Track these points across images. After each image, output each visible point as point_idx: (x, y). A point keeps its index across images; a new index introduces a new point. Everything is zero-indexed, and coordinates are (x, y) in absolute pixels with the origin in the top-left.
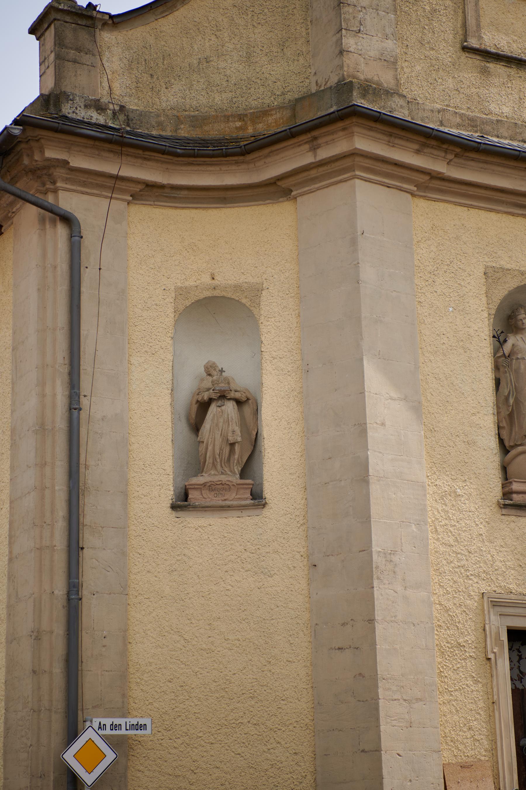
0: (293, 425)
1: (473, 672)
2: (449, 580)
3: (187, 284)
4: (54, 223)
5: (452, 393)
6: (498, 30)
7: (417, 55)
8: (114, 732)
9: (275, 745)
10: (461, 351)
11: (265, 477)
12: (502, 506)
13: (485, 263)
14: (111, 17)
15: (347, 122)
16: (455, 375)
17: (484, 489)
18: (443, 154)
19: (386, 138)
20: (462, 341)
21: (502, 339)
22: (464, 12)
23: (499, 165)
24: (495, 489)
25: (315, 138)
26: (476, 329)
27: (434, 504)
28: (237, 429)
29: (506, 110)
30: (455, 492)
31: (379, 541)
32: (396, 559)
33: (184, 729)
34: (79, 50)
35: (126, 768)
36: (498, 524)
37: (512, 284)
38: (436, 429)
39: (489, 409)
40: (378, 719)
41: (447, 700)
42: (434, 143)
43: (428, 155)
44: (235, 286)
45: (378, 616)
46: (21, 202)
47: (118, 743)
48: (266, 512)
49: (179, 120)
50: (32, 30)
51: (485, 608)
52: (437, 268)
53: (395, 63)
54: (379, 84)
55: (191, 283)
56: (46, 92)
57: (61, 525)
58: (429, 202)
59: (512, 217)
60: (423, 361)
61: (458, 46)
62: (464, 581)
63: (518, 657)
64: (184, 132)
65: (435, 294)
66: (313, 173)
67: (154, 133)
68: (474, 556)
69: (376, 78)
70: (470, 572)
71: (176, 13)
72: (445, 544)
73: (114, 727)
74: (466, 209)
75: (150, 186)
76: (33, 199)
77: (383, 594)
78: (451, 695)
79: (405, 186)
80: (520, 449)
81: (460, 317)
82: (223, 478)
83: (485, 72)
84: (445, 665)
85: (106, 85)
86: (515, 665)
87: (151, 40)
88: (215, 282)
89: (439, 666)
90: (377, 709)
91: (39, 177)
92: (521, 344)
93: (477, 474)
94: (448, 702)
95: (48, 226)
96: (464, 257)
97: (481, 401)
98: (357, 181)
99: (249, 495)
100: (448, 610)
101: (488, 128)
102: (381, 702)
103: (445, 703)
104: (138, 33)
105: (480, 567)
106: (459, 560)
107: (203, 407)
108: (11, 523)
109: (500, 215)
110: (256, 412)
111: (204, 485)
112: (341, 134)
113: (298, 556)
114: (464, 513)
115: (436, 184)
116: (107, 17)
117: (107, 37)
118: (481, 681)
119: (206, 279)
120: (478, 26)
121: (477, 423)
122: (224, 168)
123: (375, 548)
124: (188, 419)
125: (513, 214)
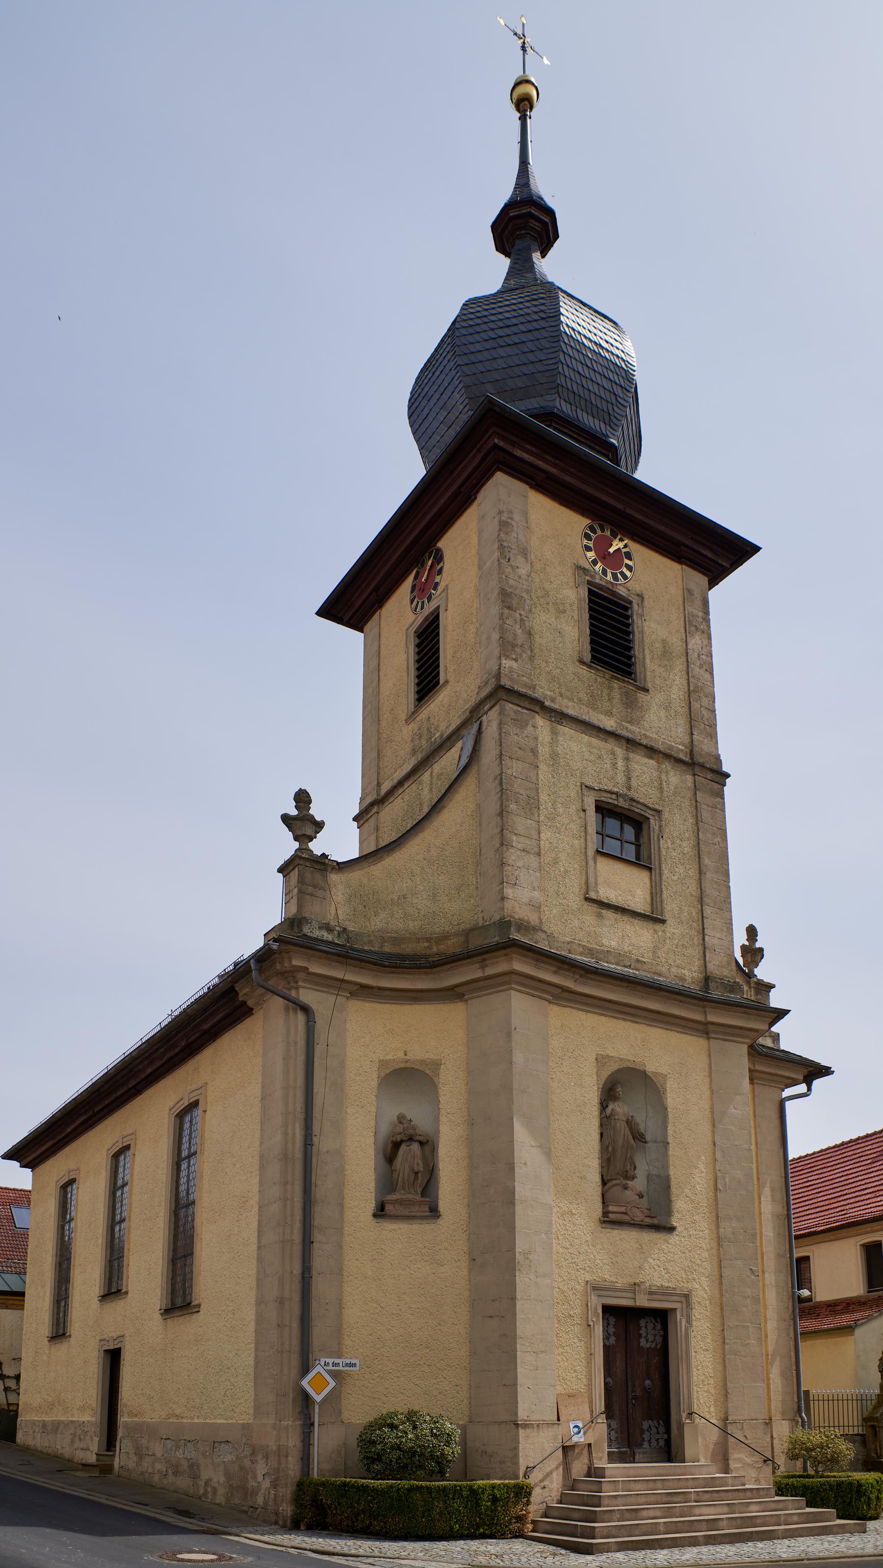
0: (461, 1161)
3: (387, 1057)
4: (295, 1011)
6: (610, 887)
7: (554, 902)
8: (334, 1368)
9: (442, 1379)
10: (579, 1113)
11: (440, 1197)
14: (338, 863)
15: (508, 950)
19: (534, 963)
21: (604, 1105)
22: (587, 873)
25: (484, 960)
28: (420, 1162)
29: (614, 944)
31: (521, 1245)
32: (530, 1257)
33: (380, 1367)
34: (315, 886)
35: (341, 1392)
37: (614, 1067)
40: (516, 1365)
42: (566, 967)
44: (421, 1061)
45: (518, 1296)
46: (270, 994)
47: (335, 1375)
48: (440, 1221)
49: (383, 940)
50: (280, 870)
53: (539, 907)
54: (528, 922)
55: (390, 1057)
56: (290, 915)
57: (298, 1226)
61: (582, 897)
64: (387, 948)
66: (481, 984)
67: (366, 948)
69: (526, 918)
71: (383, 862)
73: (334, 1364)
75: (363, 987)
76: (282, 994)
77: (522, 1281)
79: (545, 996)
80: (614, 1182)
82: (410, 1196)
83: (600, 916)
85: (333, 912)
87: (365, 881)
88: (407, 1057)
90: (516, 1358)
91: (286, 978)
92: (618, 1109)
95: (291, 1013)
98: (513, 992)
99: (427, 1209)
101: (601, 956)
102: (518, 1353)
104: (356, 875)
106: (573, 1258)
107: (396, 1145)
108: (260, 1221)
110: (434, 1150)
111: (397, 1200)
112: (503, 958)
113: (462, 1253)
115: (566, 995)
116: (335, 864)
117: (334, 878)
119: (401, 1055)
120: (596, 884)
122: (417, 976)
123: (518, 1250)
124: (384, 1154)
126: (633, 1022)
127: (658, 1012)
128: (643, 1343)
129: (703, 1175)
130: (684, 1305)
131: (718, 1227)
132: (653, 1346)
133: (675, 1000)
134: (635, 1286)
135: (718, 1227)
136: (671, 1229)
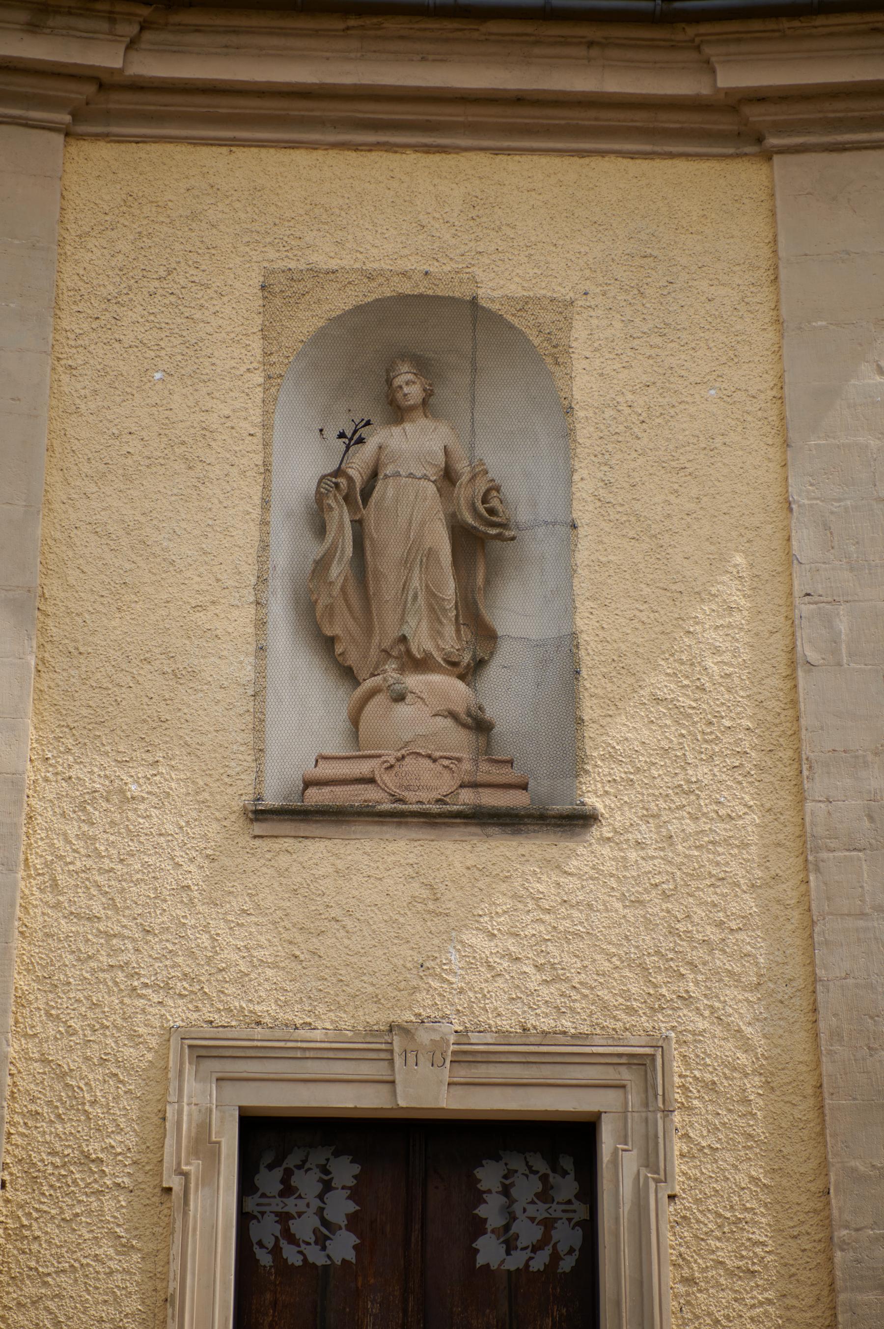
1: (118, 1225)
2: (78, 1001)
5: (142, 564)
10: (180, 466)
12: (250, 815)
13: (266, 264)
16: (155, 522)
17: (208, 780)
18: (105, 26)
20: (183, 443)
23: (271, 32)
24: (242, 777)
26: (227, 412)
27: (59, 824)
30: (122, 792)
36: (240, 860)
38: (82, 649)
39: (245, 592)
41: (30, 1297)
43: (64, 32)
51: (171, 1064)
52: (130, 288)
58: (123, 147)
59: (354, 154)
60: (64, 498)
62: (122, 1002)
63: (320, 1186)
65: (117, 345)
68: (161, 941)
70: (142, 980)
72: (78, 916)
74: (224, 150)
78: (46, 1284)
81: (184, 391)
84: (37, 1210)
86: (308, 1205)
89: (20, 1213)
93: (194, 746)
94: (33, 1303)
96: (207, 257)
97: (224, 577)
100: (65, 1074)
103: (24, 1306)
105: (175, 965)
109: (320, 152)
114: (142, 839)
118: (139, 1245)
121: (207, 626)
125: (356, 147)
126: (428, 149)
127: (519, 100)
128: (489, 1251)
129: (737, 617)
130: (634, 1098)
131: (801, 798)
132: (539, 1263)
133: (564, 42)
134: (390, 1041)
135: (801, 798)
136: (578, 821)
